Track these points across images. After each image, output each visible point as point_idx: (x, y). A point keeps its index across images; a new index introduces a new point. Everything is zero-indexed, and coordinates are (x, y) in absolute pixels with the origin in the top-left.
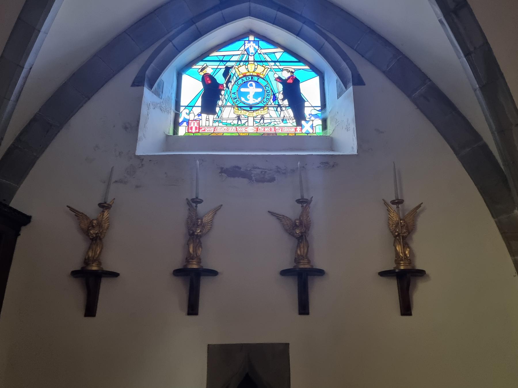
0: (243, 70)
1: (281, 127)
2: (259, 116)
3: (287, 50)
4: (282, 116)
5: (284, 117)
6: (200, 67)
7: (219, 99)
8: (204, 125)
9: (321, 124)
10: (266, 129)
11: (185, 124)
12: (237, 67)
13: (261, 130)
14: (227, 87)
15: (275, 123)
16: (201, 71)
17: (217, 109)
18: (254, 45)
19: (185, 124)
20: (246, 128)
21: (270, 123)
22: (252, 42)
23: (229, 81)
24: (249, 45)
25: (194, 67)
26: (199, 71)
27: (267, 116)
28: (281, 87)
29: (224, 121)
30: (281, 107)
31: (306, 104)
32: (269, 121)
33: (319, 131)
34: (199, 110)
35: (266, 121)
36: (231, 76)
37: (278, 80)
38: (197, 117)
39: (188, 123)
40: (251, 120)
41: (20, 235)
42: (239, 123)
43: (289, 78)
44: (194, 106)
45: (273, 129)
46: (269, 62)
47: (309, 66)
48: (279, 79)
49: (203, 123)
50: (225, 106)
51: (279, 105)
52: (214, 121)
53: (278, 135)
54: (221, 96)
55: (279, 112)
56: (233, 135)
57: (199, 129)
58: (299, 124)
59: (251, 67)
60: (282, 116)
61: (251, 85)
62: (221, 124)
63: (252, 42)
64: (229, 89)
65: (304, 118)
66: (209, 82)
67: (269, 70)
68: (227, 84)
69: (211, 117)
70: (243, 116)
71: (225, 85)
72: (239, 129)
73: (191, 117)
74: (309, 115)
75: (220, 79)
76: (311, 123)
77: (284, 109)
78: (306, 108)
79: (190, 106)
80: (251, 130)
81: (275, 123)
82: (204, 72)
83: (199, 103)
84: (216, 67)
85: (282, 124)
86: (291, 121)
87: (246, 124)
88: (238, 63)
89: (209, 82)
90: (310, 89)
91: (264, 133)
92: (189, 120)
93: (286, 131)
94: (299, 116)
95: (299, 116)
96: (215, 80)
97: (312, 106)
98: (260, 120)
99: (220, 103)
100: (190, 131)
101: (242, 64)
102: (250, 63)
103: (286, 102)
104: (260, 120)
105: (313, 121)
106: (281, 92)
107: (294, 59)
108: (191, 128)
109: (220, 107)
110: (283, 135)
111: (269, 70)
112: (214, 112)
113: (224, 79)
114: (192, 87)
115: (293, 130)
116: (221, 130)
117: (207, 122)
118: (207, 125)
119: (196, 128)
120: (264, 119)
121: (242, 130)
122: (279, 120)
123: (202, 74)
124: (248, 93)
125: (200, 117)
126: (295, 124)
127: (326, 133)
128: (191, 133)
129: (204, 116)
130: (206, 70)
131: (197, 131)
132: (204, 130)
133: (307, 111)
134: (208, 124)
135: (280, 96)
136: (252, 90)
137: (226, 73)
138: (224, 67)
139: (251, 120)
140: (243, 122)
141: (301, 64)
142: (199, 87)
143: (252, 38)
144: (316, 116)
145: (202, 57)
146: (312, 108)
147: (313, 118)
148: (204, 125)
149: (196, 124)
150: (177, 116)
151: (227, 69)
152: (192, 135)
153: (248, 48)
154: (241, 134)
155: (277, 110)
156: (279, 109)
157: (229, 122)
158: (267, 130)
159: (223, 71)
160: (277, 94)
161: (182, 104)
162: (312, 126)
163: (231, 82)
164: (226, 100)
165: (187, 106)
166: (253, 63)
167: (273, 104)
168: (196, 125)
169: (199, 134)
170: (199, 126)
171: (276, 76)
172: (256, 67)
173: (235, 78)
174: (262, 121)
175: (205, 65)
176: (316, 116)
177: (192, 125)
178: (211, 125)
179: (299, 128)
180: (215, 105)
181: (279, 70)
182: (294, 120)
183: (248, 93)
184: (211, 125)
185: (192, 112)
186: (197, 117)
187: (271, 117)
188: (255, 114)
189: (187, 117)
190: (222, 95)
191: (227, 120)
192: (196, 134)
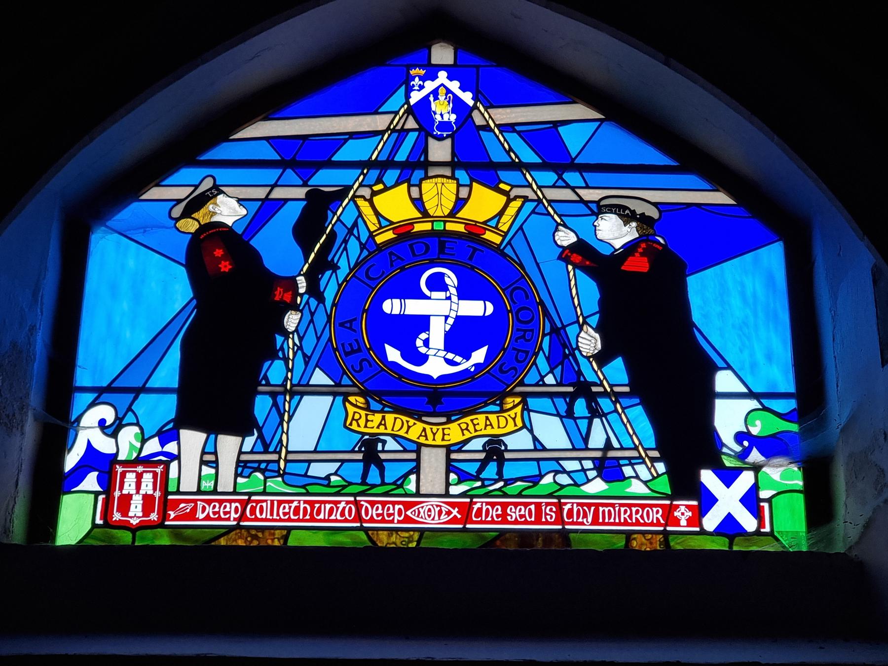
0: (396, 204)
1: (594, 503)
2: (477, 444)
3: (617, 109)
4: (597, 439)
5: (608, 446)
6: (181, 193)
7: (272, 353)
8: (189, 484)
9: (799, 483)
10: (514, 514)
11: (91, 482)
12: (366, 192)
13: (488, 518)
14: (315, 291)
15: (563, 479)
16: (187, 213)
17: (262, 406)
18: (454, 86)
19: (91, 482)
20: (408, 506)
21: (535, 480)
22: (443, 75)
23: (323, 264)
24: (430, 86)
25: (154, 193)
26: (177, 212)
27: (519, 441)
28: (587, 292)
29: (291, 468)
30: (592, 399)
31: (724, 381)
32: (531, 469)
33: (790, 523)
34: (165, 408)
35: (510, 471)
36: (333, 235)
37: (577, 258)
38: (153, 446)
39: (107, 483)
40: (433, 463)
41: (437, 77)
42: (374, 476)
43: (630, 247)
44: (143, 389)
45: (550, 514)
46: (530, 167)
47: (730, 193)
48: (583, 255)
49: (187, 474)
50: (303, 389)
51: (584, 389)
52: (243, 467)
53: (577, 544)
54: (279, 339)
55: (583, 424)
56: (343, 540)
57: (166, 505)
58: (684, 484)
59: (439, 194)
60: (597, 439)
61: (437, 284)
62: (276, 484)
63: (443, 75)
64: (321, 299)
65: (708, 450)
66: (225, 267)
67: (529, 206)
68: (313, 277)
69: (229, 446)
70: (391, 445)
71: (302, 284)
72: (373, 512)
73: (127, 443)
74: (739, 437)
75: (278, 249)
76: (745, 480)
77: (605, 404)
78: (719, 403)
79: (123, 391)
80: (432, 515)
81: (563, 479)
82: (202, 216)
83: (169, 372)
84: (261, 193)
85: (597, 486)
86: (642, 471)
87: (411, 487)
88: (374, 174)
89: (225, 267)
90: (738, 308)
91: (502, 532)
92: (112, 459)
93: (617, 520)
94: (688, 447)
95: (688, 447)
96: (256, 256)
97: (751, 394)
98: (484, 463)
99: (275, 372)
100: (117, 516)
101: (391, 175)
102: (432, 172)
103: (617, 372)
104: (484, 463)
105: (756, 468)
106: (594, 320)
107: (654, 156)
108: (126, 500)
109: (274, 395)
110: (600, 544)
111: (529, 206)
112: (243, 424)
113: (298, 251)
114: (135, 293)
115: (656, 515)
116: (277, 510)
117: (207, 471)
118: (207, 485)
119: (148, 500)
120: (501, 462)
121: (386, 518)
122: (570, 465)
123: (190, 226)
124: (423, 323)
125: (172, 447)
126: (664, 485)
127: (829, 540)
128: (124, 526)
129: (192, 441)
130: (210, 207)
131: (154, 516)
132: (192, 515)
133: (729, 419)
134: (204, 468)
135: (589, 342)
136: (440, 308)
137: (308, 228)
138: (301, 192)
139: (433, 463)
140: (393, 472)
141: (692, 179)
142: (172, 291)
143: (442, 54)
144: (772, 446)
145: (194, 142)
146: (753, 404)
147: (755, 456)
148: (189, 484)
149: (148, 478)
150: (58, 430)
151: (320, 204)
152: (126, 537)
153: (426, 99)
154: (383, 540)
155: (570, 413)
156: (580, 407)
157: (318, 470)
158: (519, 519)
159: (291, 214)
160: (572, 331)
161: (82, 378)
162: (756, 501)
163: (335, 268)
164: (307, 359)
165: (110, 389)
166: (447, 172)
167: (550, 379)
168: (147, 486)
169: (164, 539)
170: (165, 492)
171: (566, 238)
172: (463, 193)
173: (354, 247)
174: (491, 471)
175: (208, 184)
176: (772, 446)
177: (129, 487)
178: (226, 484)
179: (683, 510)
180: (252, 383)
181: (584, 210)
182: (661, 467)
183: (423, 323)
184: (226, 484)
185: (130, 418)
186: (153, 446)
187: (538, 445)
188: (454, 433)
189: (105, 445)
190: (286, 334)
191: (310, 464)
192: (145, 539)
